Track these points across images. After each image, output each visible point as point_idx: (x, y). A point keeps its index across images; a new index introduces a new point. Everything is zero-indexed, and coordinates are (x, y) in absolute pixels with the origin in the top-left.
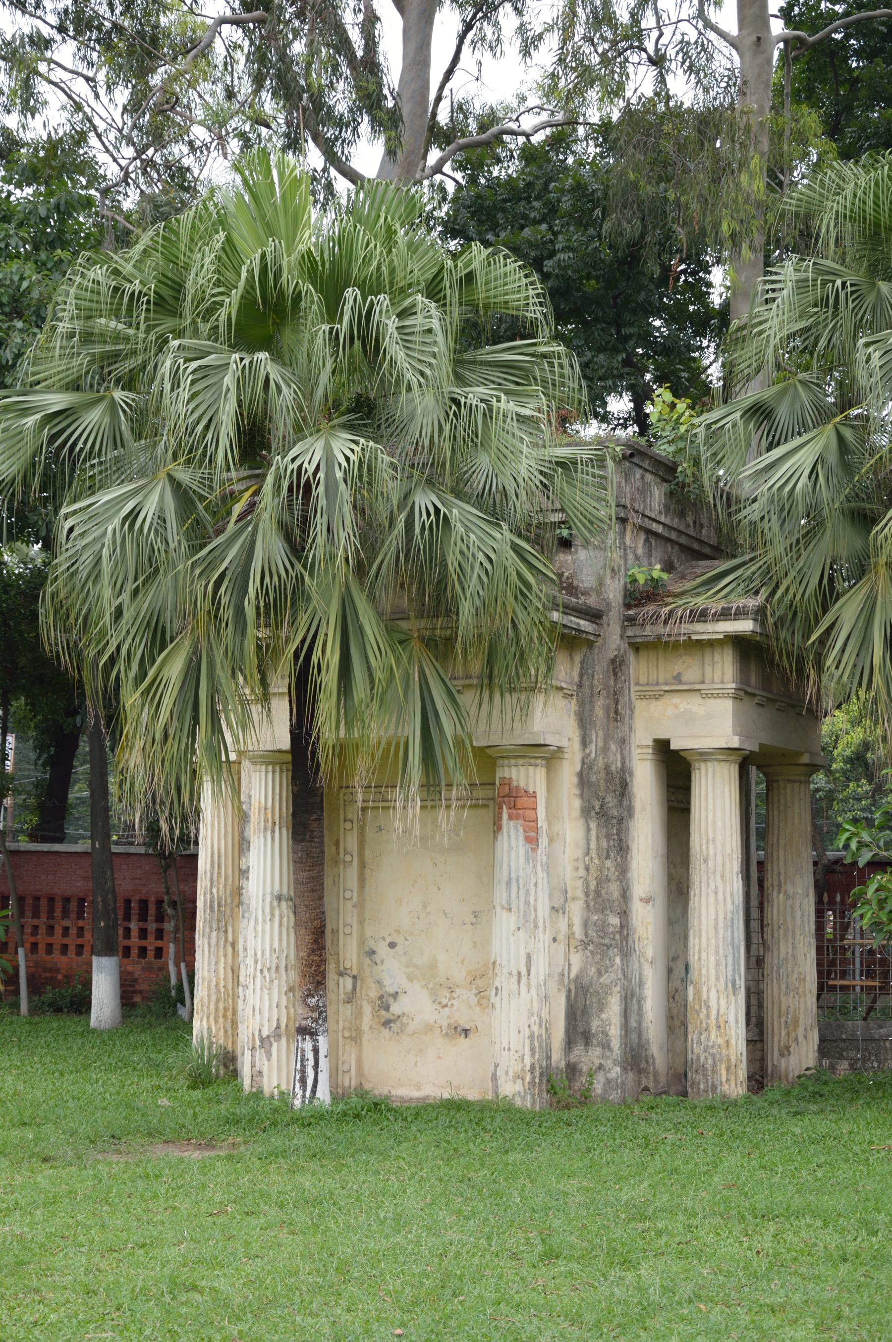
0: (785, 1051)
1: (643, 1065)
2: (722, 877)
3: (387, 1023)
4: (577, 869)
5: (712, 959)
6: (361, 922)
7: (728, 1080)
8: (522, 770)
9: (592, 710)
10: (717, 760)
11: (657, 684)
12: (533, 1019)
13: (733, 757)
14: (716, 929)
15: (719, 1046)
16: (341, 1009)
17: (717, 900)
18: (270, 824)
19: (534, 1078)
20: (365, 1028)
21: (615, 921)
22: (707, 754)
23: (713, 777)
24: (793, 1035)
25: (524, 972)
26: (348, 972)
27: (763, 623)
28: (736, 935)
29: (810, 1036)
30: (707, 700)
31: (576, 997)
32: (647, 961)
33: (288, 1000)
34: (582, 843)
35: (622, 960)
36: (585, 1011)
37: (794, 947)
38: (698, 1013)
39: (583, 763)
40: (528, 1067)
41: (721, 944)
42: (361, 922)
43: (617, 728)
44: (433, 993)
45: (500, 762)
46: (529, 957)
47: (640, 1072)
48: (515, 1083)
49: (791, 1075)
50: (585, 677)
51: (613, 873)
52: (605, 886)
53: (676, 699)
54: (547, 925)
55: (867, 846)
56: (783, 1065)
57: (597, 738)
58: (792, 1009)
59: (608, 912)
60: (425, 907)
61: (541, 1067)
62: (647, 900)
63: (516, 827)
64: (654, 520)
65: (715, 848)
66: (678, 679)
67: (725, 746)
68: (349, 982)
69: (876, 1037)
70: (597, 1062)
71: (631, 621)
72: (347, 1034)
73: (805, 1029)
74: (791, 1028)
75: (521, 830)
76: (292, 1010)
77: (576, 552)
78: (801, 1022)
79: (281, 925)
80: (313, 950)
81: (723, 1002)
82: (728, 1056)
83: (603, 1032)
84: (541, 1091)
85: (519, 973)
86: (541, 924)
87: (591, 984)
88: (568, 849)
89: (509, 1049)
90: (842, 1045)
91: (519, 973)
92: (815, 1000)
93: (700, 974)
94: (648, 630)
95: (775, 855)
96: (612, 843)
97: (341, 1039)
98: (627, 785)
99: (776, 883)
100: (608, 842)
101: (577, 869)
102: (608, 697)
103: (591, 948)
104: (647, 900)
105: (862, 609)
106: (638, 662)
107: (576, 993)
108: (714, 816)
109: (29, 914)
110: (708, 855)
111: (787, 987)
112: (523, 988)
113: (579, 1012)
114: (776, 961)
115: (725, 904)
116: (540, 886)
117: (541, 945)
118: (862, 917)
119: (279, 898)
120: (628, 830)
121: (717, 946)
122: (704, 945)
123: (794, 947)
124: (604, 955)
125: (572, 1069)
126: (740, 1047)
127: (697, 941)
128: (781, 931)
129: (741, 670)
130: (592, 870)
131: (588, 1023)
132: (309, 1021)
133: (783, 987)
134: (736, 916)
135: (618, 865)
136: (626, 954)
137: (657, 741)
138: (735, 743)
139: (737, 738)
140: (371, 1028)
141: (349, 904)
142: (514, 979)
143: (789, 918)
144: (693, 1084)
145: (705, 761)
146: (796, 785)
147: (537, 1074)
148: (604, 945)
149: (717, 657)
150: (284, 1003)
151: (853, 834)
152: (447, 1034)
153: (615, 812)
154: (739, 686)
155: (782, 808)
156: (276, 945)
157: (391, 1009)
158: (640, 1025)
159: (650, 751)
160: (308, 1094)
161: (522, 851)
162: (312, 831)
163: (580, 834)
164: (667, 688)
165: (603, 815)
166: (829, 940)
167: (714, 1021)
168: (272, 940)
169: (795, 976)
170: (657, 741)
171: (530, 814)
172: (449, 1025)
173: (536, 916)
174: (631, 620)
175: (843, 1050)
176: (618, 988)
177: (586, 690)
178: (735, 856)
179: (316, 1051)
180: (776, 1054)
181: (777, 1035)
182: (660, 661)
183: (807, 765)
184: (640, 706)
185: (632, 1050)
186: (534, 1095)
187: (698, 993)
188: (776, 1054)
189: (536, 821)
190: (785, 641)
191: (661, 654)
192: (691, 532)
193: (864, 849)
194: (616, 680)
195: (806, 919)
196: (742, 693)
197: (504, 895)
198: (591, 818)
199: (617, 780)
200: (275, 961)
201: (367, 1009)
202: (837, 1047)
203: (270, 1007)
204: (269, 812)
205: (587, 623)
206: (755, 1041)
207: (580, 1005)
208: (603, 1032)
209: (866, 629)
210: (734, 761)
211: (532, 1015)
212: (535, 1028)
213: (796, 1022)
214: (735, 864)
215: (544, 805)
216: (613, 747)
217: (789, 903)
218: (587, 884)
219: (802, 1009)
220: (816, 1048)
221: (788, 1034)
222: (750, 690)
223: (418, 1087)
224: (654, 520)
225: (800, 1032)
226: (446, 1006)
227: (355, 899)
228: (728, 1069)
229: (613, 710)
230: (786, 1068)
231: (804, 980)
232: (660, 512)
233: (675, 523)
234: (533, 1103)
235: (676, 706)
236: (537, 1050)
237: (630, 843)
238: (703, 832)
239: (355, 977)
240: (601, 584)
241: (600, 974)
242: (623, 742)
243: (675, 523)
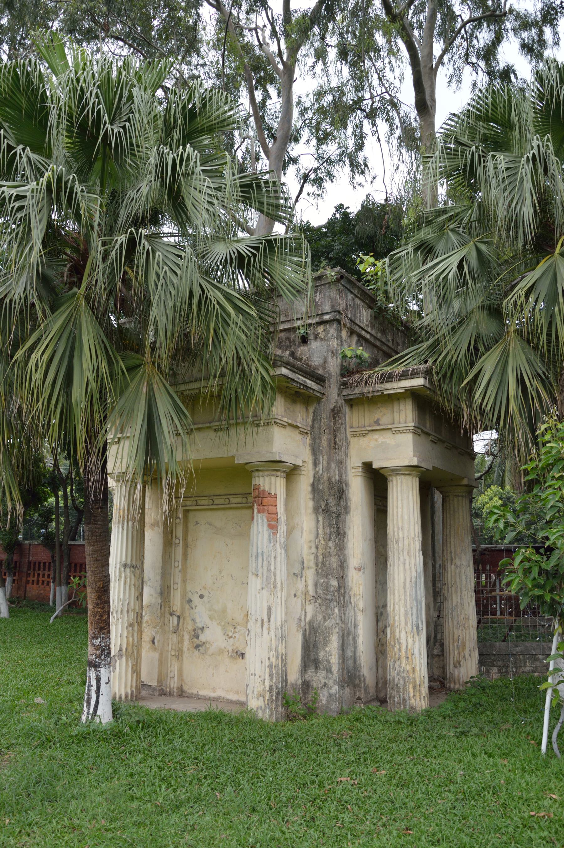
0: (458, 664)
1: (357, 682)
2: (408, 553)
3: (197, 647)
4: (311, 547)
5: (402, 610)
6: (184, 581)
7: (414, 696)
8: (267, 479)
9: (320, 442)
10: (403, 474)
11: (364, 427)
12: (271, 653)
13: (414, 473)
14: (404, 588)
15: (408, 672)
16: (171, 637)
17: (405, 569)
18: (121, 519)
19: (272, 696)
20: (185, 649)
21: (334, 583)
22: (396, 470)
23: (401, 486)
24: (462, 654)
25: (266, 619)
26: (175, 613)
27: (430, 381)
28: (419, 593)
29: (473, 654)
30: (396, 435)
31: (309, 635)
32: (359, 610)
33: (128, 632)
34: (314, 530)
35: (339, 610)
36: (315, 645)
37: (461, 598)
38: (393, 647)
39: (314, 477)
40: (267, 689)
41: (408, 599)
42: (184, 581)
43: (336, 453)
44: (224, 629)
45: (256, 474)
46: (269, 609)
47: (355, 686)
48: (258, 699)
49: (461, 680)
50: (316, 422)
51: (333, 551)
52: (328, 559)
53: (376, 436)
54: (285, 586)
55: (512, 526)
56: (456, 673)
57: (323, 460)
58: (461, 638)
59: (330, 577)
60: (220, 572)
61: (277, 688)
62: (359, 569)
63: (262, 518)
64: (363, 329)
65: (403, 533)
66: (377, 422)
67: (408, 464)
68: (176, 619)
69: (514, 652)
70: (323, 681)
71: (345, 384)
72: (173, 654)
73: (470, 651)
74: (461, 650)
75: (265, 520)
76: (131, 639)
77: (310, 344)
78: (467, 645)
79: (125, 583)
80: (97, 604)
81: (410, 640)
82: (414, 678)
83: (327, 661)
84: (277, 706)
85: (262, 620)
86: (279, 585)
87: (319, 626)
88: (304, 534)
89: (255, 675)
90: (493, 657)
91: (262, 620)
92: (475, 632)
93: (394, 620)
94: (357, 391)
95: (448, 541)
96: (332, 530)
97: (170, 656)
98: (343, 491)
99: (449, 558)
100: (330, 529)
101: (311, 547)
102: (330, 434)
103: (319, 601)
104: (359, 569)
105: (499, 360)
106: (352, 413)
107: (310, 632)
108: (402, 512)
109: (73, 571)
110: (398, 538)
111: (458, 623)
112: (265, 631)
113: (311, 646)
114: (450, 607)
115: (411, 572)
116: (278, 559)
117: (279, 601)
118: (509, 584)
119: (125, 566)
120: (344, 521)
121: (405, 601)
122: (397, 600)
123: (461, 598)
124: (327, 606)
125: (306, 685)
126: (422, 672)
127: (392, 597)
128: (453, 588)
129: (419, 413)
130: (320, 548)
131: (317, 654)
132: (94, 657)
133: (455, 623)
134: (418, 580)
135: (337, 545)
136: (343, 605)
137: (364, 463)
138: (415, 462)
139: (416, 459)
140: (188, 649)
141: (177, 570)
142: (259, 624)
143: (458, 580)
144: (390, 697)
145: (396, 475)
146: (460, 498)
147: (274, 693)
148: (327, 599)
149: (402, 406)
150: (125, 634)
151: (500, 516)
152: (231, 656)
153: (334, 509)
154: (416, 425)
155: (452, 512)
156: (121, 596)
157: (200, 638)
158: (355, 654)
159: (360, 470)
160: (91, 711)
161: (266, 534)
162: (96, 516)
163: (313, 524)
164: (370, 429)
165: (327, 511)
166: (483, 586)
167: (404, 654)
168: (119, 592)
169: (463, 616)
170: (364, 463)
171: (272, 509)
172: (233, 650)
173: (275, 580)
174: (345, 384)
175: (493, 660)
176: (337, 630)
177: (316, 430)
178: (417, 539)
179: (98, 679)
180: (452, 666)
181: (453, 654)
182: (366, 413)
183: (466, 486)
184: (354, 442)
185: (349, 672)
186: (272, 709)
187: (393, 633)
188: (452, 666)
189: (276, 514)
190: (446, 391)
191: (366, 406)
192: (390, 344)
193: (509, 529)
194: (335, 422)
195: (468, 580)
196: (419, 431)
197: (254, 565)
198: (319, 513)
199: (336, 488)
200: (120, 607)
201: (186, 637)
202: (490, 659)
203: (116, 636)
204: (122, 511)
205: (313, 383)
206: (440, 656)
207: (312, 640)
208: (327, 661)
209: (502, 374)
210: (415, 475)
211: (271, 650)
212: (273, 660)
213: (464, 646)
214: (417, 545)
215: (282, 503)
216: (333, 466)
217: (458, 570)
218: (317, 557)
219: (467, 637)
220: (477, 662)
221: (459, 653)
222: (425, 430)
223: (214, 690)
224: (363, 329)
225: (467, 652)
226: (231, 637)
227: (180, 567)
228: (414, 688)
229: (333, 441)
230: (459, 675)
231: (469, 619)
232: (367, 325)
233: (379, 335)
234: (271, 716)
235: (376, 440)
236: (274, 676)
237: (346, 530)
238: (395, 522)
239: (179, 617)
240: (325, 362)
241: (325, 619)
242: (340, 463)
243: (379, 335)
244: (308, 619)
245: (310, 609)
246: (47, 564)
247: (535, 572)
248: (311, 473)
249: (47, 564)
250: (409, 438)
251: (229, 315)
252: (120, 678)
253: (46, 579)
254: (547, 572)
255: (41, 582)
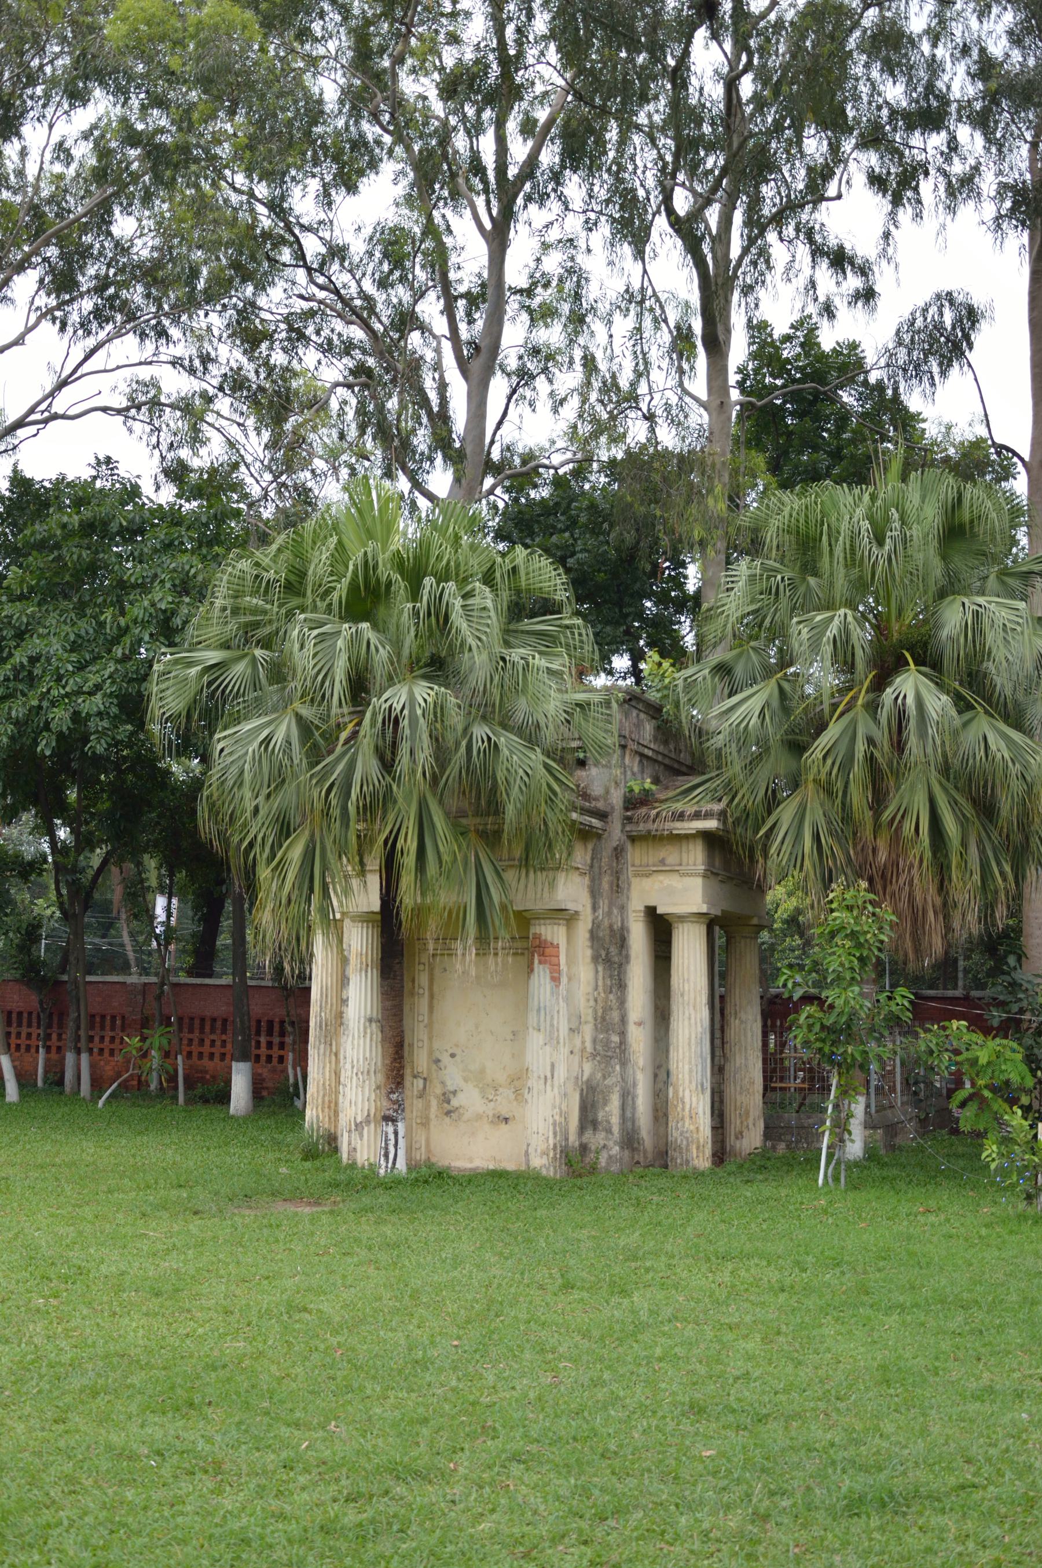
0: (740, 1135)
3: (448, 1113)
5: (687, 1067)
6: (430, 1038)
8: (549, 927)
9: (600, 884)
20: (432, 1116)
25: (549, 1075)
27: (725, 823)
36: (593, 1105)
37: (746, 1059)
38: (676, 1107)
42: (430, 1038)
46: (553, 1066)
51: (614, 1004)
53: (661, 877)
57: (603, 904)
60: (477, 1027)
66: (662, 862)
68: (421, 1082)
70: (602, 1143)
81: (694, 1099)
94: (642, 827)
109: (55, 1025)
118: (795, 1037)
119: (370, 1020)
125: (584, 1148)
131: (596, 1114)
138: (704, 909)
141: (422, 1025)
142: (542, 1081)
150: (373, 1097)
153: (616, 959)
163: (591, 975)
165: (608, 961)
174: (629, 819)
177: (596, 869)
179: (396, 1133)
181: (734, 1123)
184: (635, 882)
187: (676, 1092)
192: (673, 755)
201: (434, 1103)
212: (557, 1118)
213: (747, 1113)
214: (703, 998)
216: (615, 911)
218: (595, 1011)
223: (471, 1160)
225: (751, 1121)
228: (698, 1148)
234: (555, 1173)
240: (607, 792)
241: (604, 1077)
242: (623, 908)
243: (661, 749)
244: (585, 1078)
245: (588, 1068)
246: (25, 1015)
247: (817, 1028)
248: (590, 919)
249: (25, 1015)
250: (699, 881)
251: (555, 794)
252: (369, 1146)
253: (23, 1041)
254: (828, 1028)
255: (13, 1046)
